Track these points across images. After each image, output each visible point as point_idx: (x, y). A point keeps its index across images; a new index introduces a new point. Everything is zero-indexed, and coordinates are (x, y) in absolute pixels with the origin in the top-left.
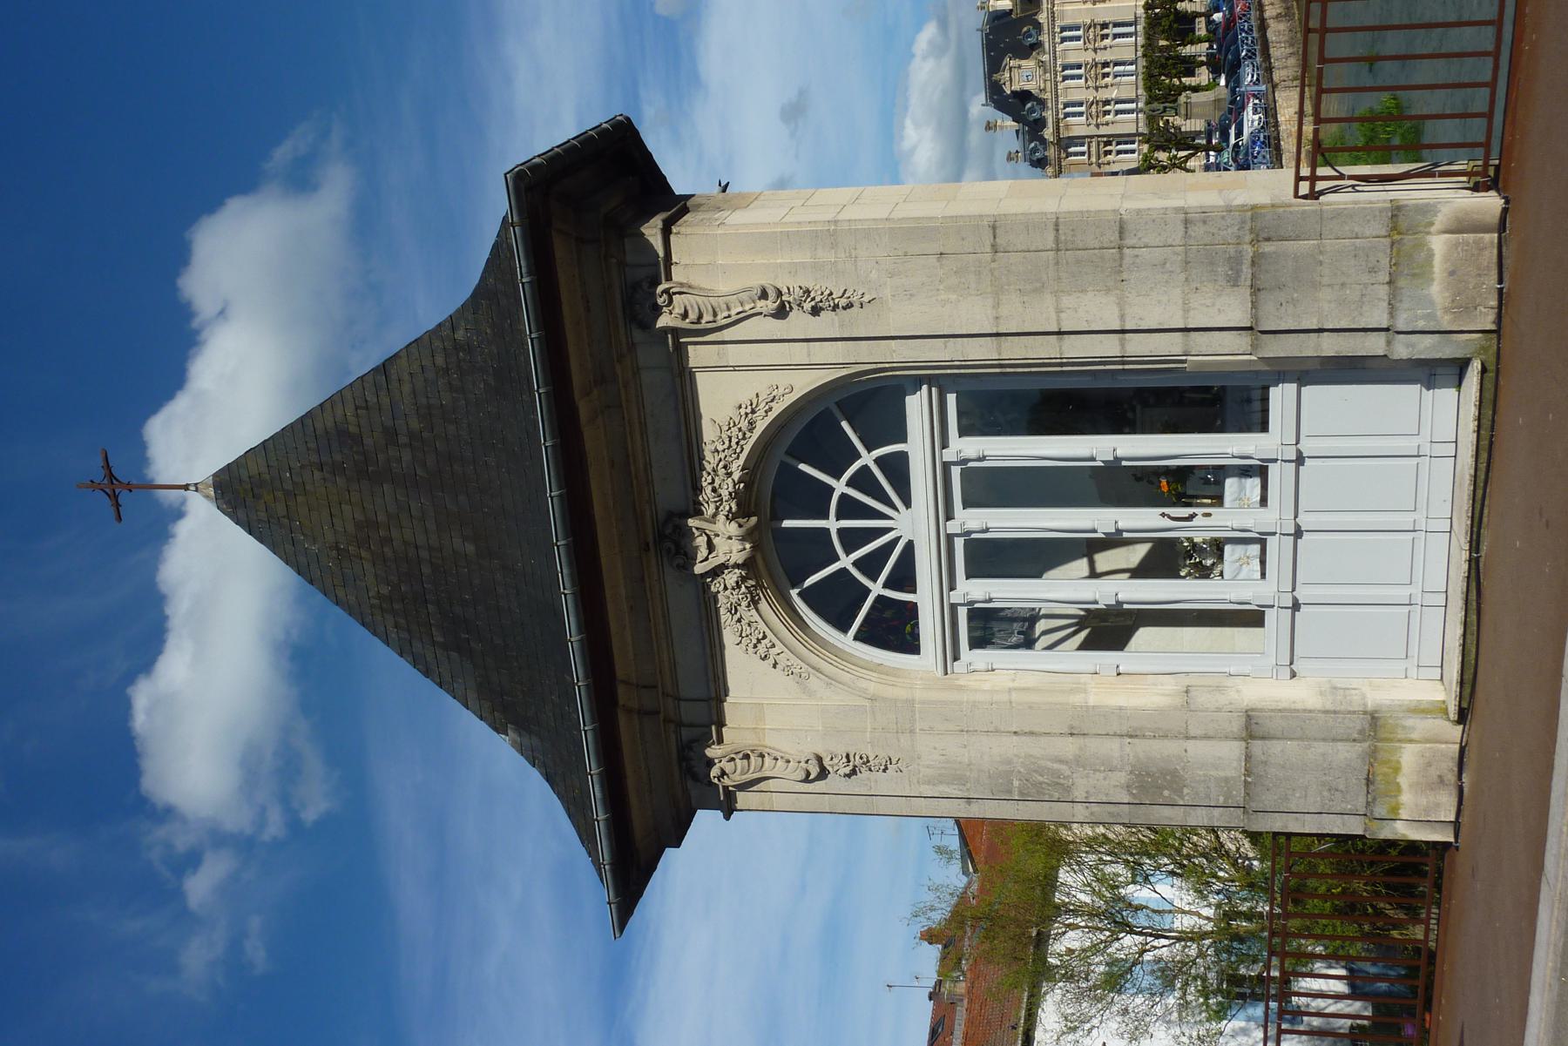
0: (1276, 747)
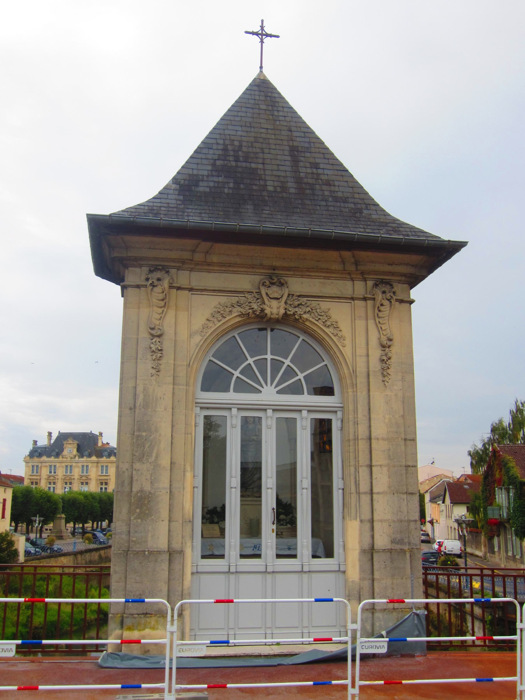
0: (165, 566)
